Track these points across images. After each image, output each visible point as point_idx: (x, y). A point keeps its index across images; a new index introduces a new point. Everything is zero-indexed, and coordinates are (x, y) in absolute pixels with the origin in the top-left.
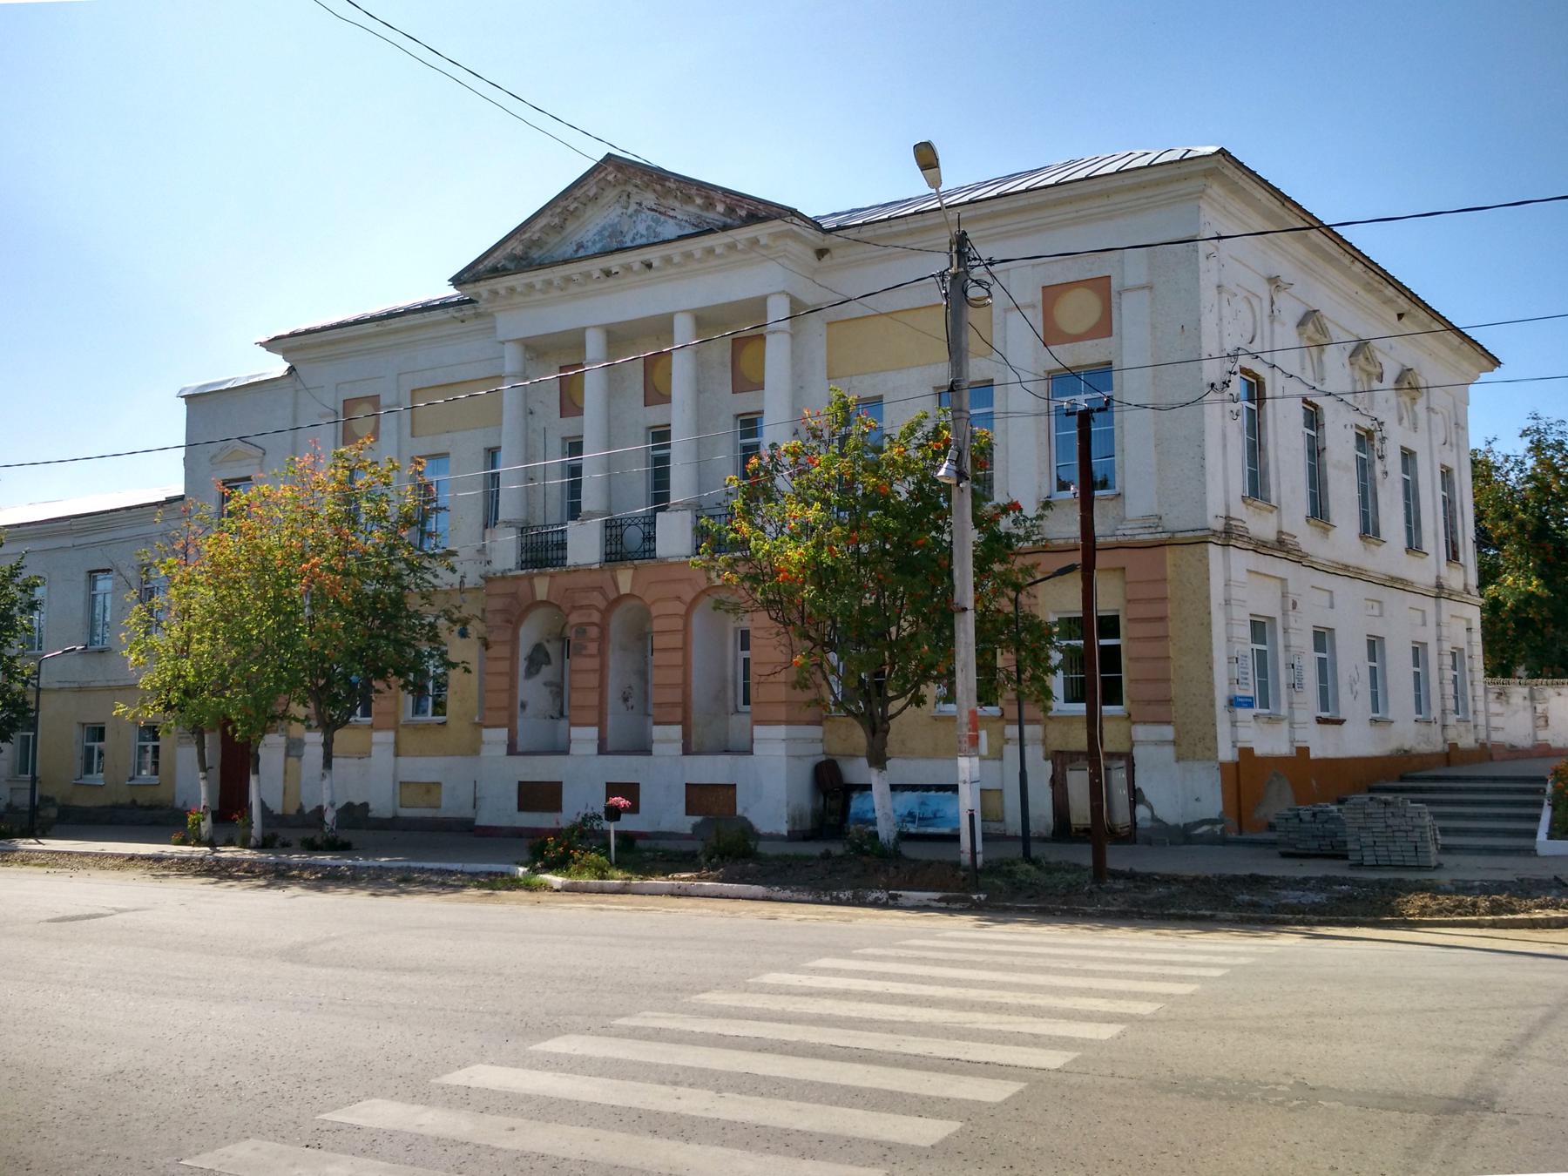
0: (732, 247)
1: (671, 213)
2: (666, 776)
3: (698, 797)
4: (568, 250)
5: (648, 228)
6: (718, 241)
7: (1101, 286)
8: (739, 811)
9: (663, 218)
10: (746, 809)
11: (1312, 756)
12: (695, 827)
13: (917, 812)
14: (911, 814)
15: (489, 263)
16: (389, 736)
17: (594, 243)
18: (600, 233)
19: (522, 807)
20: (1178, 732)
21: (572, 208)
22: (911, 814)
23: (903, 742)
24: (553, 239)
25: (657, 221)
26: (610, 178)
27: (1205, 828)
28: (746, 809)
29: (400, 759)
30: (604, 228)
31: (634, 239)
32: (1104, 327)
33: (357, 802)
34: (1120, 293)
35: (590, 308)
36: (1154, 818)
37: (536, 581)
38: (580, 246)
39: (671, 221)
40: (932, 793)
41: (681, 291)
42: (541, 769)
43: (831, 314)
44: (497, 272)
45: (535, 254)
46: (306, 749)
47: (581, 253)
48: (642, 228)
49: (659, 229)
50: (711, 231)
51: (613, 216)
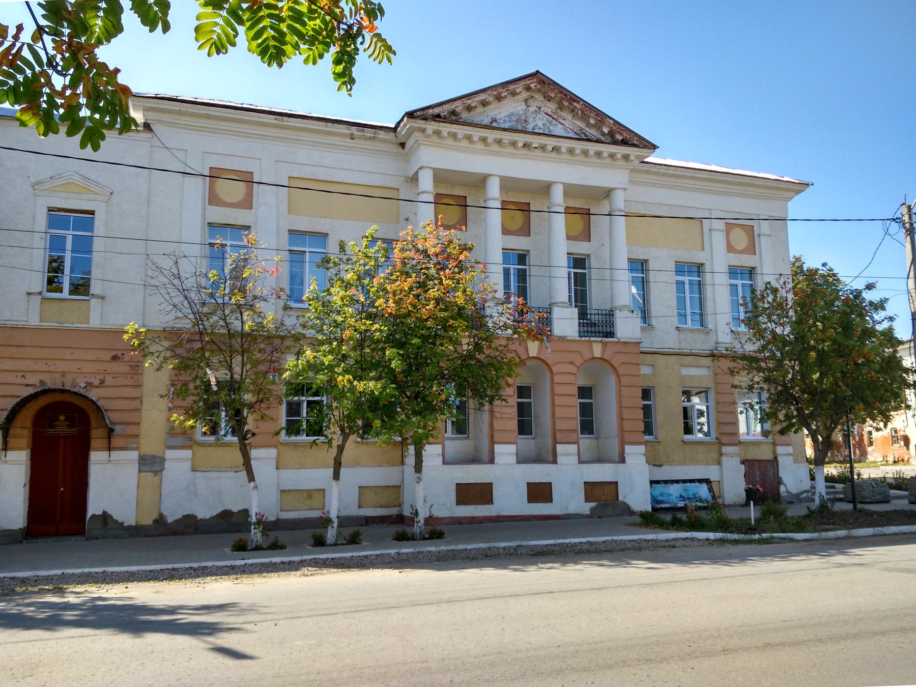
0: (612, 156)
1: (562, 121)
2: (570, 476)
3: (592, 489)
4: (486, 121)
5: (544, 125)
6: (593, 147)
7: (750, 231)
8: (621, 498)
9: (554, 122)
10: (625, 497)
11: (170, 520)
12: (592, 510)
13: (684, 495)
14: (681, 496)
15: (436, 111)
16: (273, 452)
17: (505, 121)
18: (509, 116)
19: (460, 502)
20: (794, 450)
21: (503, 95)
22: (681, 496)
23: (668, 456)
24: (480, 109)
25: (551, 123)
26: (532, 86)
27: (805, 494)
28: (625, 497)
29: (281, 471)
30: (512, 114)
31: (534, 128)
32: (247, 203)
33: (235, 509)
34: (759, 236)
35: (498, 165)
36: (788, 492)
37: (594, 345)
38: (494, 120)
39: (560, 126)
40: (688, 484)
41: (563, 171)
42: (474, 474)
43: (727, 221)
44: (437, 118)
45: (465, 115)
46: (167, 464)
47: (495, 124)
48: (540, 124)
49: (551, 128)
50: (589, 140)
51: (519, 109)
